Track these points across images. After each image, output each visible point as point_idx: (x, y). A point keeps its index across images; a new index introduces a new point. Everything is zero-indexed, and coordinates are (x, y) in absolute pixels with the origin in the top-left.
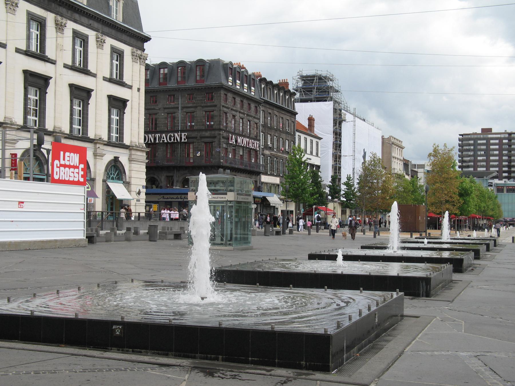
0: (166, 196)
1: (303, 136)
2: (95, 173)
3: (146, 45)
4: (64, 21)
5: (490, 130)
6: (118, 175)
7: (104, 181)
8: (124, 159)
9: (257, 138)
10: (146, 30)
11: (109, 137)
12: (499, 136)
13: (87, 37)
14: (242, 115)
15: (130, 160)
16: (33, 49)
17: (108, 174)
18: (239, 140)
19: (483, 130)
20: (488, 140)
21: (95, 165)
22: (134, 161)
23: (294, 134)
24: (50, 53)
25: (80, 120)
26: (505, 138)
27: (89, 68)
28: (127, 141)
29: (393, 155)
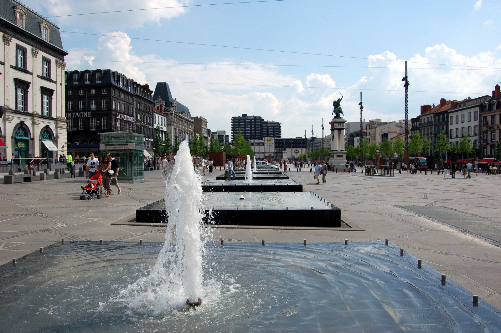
0: (79, 149)
1: (157, 115)
2: (34, 135)
3: (65, 57)
4: (10, 38)
5: (246, 115)
6: (49, 136)
7: (40, 140)
8: (28, 122)
9: (132, 116)
10: (65, 49)
11: (42, 113)
12: (250, 118)
13: (26, 49)
14: (123, 102)
15: (57, 127)
16: (20, 66)
17: (42, 135)
18: (123, 116)
19: (243, 115)
20: (245, 120)
21: (33, 130)
22: (59, 128)
23: (153, 114)
24: (29, 68)
25: (22, 101)
26: (253, 119)
27: (52, 78)
28: (54, 115)
29: (202, 126)
